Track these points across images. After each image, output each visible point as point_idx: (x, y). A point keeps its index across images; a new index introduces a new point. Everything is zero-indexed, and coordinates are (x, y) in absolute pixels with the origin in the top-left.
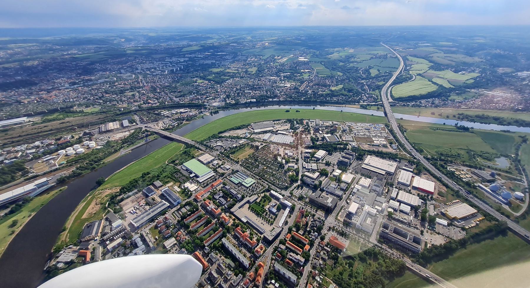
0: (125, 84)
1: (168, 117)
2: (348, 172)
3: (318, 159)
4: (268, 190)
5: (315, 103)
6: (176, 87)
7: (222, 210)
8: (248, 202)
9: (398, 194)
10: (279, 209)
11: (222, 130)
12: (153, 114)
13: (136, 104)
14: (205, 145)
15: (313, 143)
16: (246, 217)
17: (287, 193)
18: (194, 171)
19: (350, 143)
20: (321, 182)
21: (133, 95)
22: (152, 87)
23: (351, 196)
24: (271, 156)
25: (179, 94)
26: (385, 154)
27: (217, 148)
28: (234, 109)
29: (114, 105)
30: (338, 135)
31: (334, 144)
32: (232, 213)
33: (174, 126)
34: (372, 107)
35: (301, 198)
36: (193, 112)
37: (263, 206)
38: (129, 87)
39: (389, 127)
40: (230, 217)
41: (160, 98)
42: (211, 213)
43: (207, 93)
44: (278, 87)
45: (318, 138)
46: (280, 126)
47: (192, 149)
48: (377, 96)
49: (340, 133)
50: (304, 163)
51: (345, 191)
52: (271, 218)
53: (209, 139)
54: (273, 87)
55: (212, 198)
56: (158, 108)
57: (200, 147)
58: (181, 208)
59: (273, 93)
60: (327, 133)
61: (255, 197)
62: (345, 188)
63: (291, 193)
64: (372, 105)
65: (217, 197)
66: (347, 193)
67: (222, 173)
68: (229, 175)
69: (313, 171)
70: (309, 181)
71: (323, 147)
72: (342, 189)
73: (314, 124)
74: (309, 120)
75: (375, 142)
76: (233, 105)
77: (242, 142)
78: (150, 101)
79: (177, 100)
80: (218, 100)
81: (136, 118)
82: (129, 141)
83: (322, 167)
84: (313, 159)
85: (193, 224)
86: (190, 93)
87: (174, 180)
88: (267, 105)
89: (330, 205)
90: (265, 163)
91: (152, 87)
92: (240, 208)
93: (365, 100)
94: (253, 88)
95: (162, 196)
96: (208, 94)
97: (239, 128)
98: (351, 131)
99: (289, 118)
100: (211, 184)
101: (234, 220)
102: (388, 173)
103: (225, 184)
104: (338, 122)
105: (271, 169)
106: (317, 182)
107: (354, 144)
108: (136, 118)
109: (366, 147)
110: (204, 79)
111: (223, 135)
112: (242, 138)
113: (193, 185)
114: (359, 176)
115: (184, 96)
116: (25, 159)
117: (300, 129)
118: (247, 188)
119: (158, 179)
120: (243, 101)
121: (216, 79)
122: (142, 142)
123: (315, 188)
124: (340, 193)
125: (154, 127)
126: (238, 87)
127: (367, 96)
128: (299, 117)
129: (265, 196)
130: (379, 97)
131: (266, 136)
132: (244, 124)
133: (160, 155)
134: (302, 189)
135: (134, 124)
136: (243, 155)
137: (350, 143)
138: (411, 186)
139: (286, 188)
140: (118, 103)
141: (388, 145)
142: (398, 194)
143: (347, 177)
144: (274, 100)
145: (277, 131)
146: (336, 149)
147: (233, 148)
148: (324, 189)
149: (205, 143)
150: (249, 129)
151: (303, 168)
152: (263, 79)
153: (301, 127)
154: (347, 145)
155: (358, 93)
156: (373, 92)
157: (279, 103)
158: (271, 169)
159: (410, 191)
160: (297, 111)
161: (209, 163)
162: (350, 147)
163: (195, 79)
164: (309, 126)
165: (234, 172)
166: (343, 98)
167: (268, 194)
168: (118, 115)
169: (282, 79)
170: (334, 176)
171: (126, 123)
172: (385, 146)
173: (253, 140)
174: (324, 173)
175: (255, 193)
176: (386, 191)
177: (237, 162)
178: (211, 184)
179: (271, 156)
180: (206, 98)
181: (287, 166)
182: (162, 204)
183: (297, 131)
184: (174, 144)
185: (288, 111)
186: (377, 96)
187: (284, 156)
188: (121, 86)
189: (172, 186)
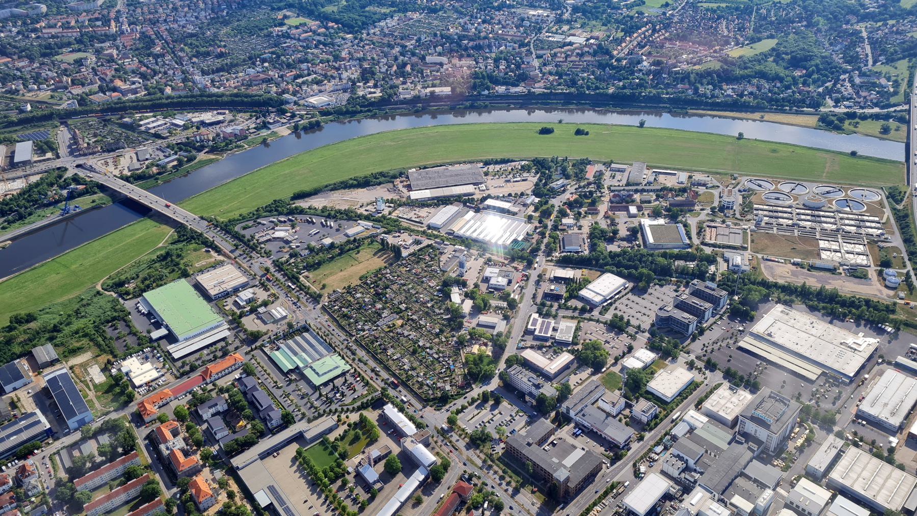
0: (66, 26)
1: (157, 136)
2: (683, 358)
3: (589, 306)
4: (378, 403)
5: (654, 105)
6: (213, 41)
7: (205, 458)
8: (299, 438)
9: (838, 457)
10: (389, 474)
11: (306, 188)
12: (114, 122)
13: (78, 90)
14: (237, 237)
15: (593, 247)
16: (272, 489)
17: (437, 418)
18: (167, 319)
19: (728, 253)
20: (565, 392)
21: (79, 63)
22: (144, 36)
23: (659, 449)
24: (433, 283)
25: (218, 63)
26: (844, 303)
27: (268, 247)
28: (374, 117)
29: (10, 92)
30: (693, 222)
31: (664, 255)
32: (233, 472)
33: (164, 167)
34: (864, 126)
35: (477, 441)
36: (244, 122)
37: (344, 456)
38: (76, 34)
39: (898, 202)
40: (223, 485)
41: (155, 73)
42: (166, 465)
43: (306, 61)
44: (541, 44)
45: (615, 232)
46: (501, 182)
47: (193, 246)
48: (896, 84)
49: (703, 216)
50: (536, 316)
51: (641, 426)
52: (355, 501)
53: (256, 216)
54: (522, 45)
55: (190, 416)
56: (135, 108)
57: (218, 242)
58: (84, 440)
59: (518, 66)
60: (656, 214)
61: (326, 422)
62: (645, 419)
63: (451, 421)
64: (864, 117)
65: (206, 413)
66: (647, 435)
67: (252, 334)
68: (272, 342)
69: (558, 346)
70: (524, 380)
71: (618, 265)
72: (634, 422)
73: (620, 180)
74: (608, 164)
75: (824, 255)
76: (372, 104)
77: (356, 229)
78: (118, 83)
79: (205, 81)
80: (329, 86)
81: (62, 136)
82: (11, 210)
83: (595, 332)
84: (573, 303)
85: (99, 496)
86: (252, 60)
87: (98, 345)
88: (488, 109)
89: (561, 475)
90: (403, 307)
91: (144, 36)
92: (264, 456)
93: (844, 98)
94: (455, 46)
95: (44, 398)
96: (304, 66)
97: (364, 183)
98: (747, 208)
99: (541, 156)
100: (203, 369)
101: (231, 495)
102: (832, 377)
103: (248, 372)
104: (709, 173)
105: (419, 328)
106: (549, 390)
107: (738, 259)
108: (62, 136)
109: (781, 272)
110: (310, 14)
111: (304, 204)
112: (361, 217)
113: (148, 366)
114: (716, 377)
115: (227, 69)
116: (894, 276)
117: (567, 196)
118: (316, 388)
119: (51, 339)
120: (408, 91)
121: (346, 17)
122: (51, 216)
123: (539, 408)
124: (618, 432)
125: (103, 169)
126: (410, 44)
127: (857, 80)
128: (573, 151)
129: (362, 423)
130: (903, 87)
131: (440, 216)
132: (384, 169)
133: (87, 262)
134: (494, 407)
135: (49, 155)
136: (338, 278)
137: (728, 253)
138: (905, 432)
139: (443, 400)
140: (25, 86)
141: (872, 273)
142: (838, 457)
143: (669, 381)
144: (514, 90)
145: (484, 199)
146: (663, 274)
147: (322, 249)
148: (572, 414)
149: (237, 228)
150: (395, 189)
151: (528, 332)
152: (499, 16)
153: (571, 189)
154: (711, 260)
155: (830, 71)
156: (885, 69)
157: (528, 102)
158: (419, 328)
159: (892, 450)
160: (579, 132)
161: (226, 295)
162: (723, 267)
163: (280, 15)
164: (599, 186)
165: (292, 332)
166: (759, 88)
167: (372, 416)
168: (11, 124)
169: (566, 16)
170: (624, 368)
171: (24, 151)
172: (857, 273)
173: (394, 226)
174: (589, 359)
175: (333, 407)
176: (800, 442)
177: (316, 298)
178: (203, 369)
179: (433, 283)
180: (297, 77)
181: (474, 322)
182: (31, 420)
183: (553, 201)
184: (144, 228)
185: (546, 131)
186: (896, 84)
187: (476, 286)
188: (53, 31)
189: (84, 366)
